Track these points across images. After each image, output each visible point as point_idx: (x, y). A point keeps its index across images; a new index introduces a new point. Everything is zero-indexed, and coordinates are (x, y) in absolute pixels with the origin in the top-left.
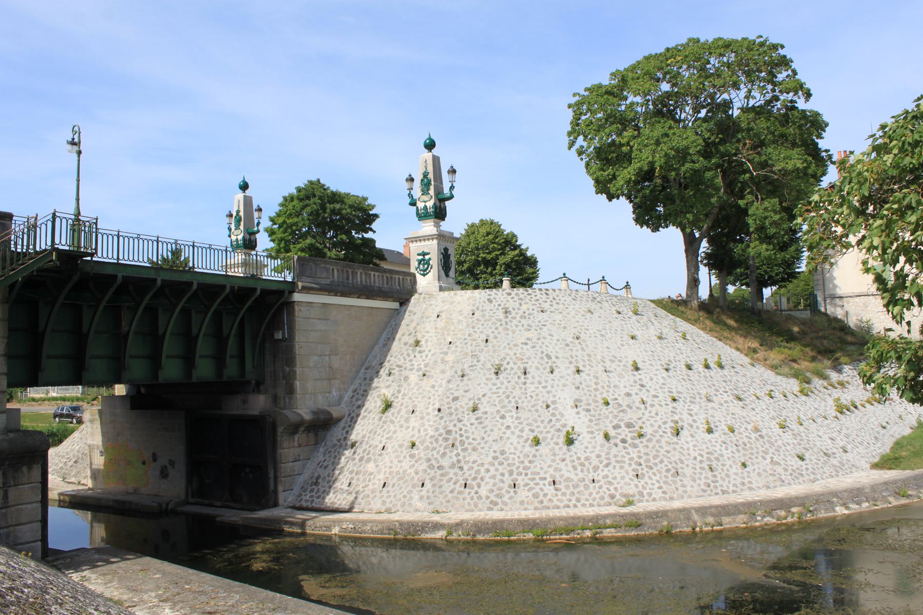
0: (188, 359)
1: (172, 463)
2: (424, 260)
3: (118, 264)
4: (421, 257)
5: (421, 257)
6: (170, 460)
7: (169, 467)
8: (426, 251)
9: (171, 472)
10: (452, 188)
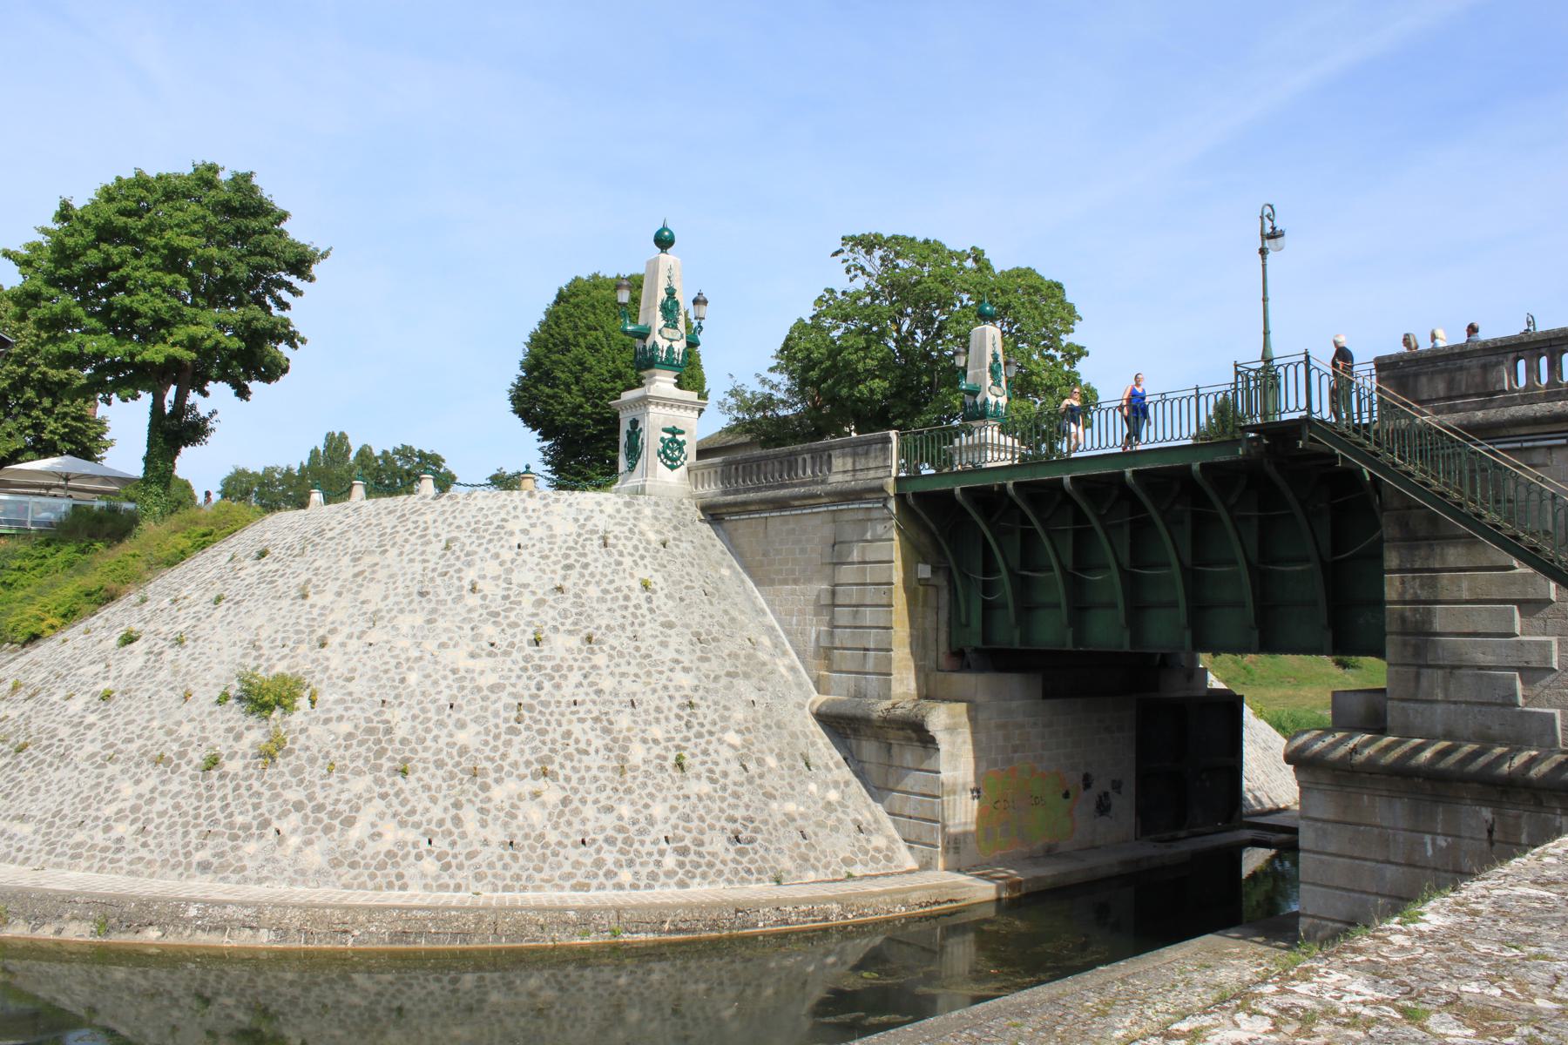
0: (1079, 609)
7: (1112, 793)
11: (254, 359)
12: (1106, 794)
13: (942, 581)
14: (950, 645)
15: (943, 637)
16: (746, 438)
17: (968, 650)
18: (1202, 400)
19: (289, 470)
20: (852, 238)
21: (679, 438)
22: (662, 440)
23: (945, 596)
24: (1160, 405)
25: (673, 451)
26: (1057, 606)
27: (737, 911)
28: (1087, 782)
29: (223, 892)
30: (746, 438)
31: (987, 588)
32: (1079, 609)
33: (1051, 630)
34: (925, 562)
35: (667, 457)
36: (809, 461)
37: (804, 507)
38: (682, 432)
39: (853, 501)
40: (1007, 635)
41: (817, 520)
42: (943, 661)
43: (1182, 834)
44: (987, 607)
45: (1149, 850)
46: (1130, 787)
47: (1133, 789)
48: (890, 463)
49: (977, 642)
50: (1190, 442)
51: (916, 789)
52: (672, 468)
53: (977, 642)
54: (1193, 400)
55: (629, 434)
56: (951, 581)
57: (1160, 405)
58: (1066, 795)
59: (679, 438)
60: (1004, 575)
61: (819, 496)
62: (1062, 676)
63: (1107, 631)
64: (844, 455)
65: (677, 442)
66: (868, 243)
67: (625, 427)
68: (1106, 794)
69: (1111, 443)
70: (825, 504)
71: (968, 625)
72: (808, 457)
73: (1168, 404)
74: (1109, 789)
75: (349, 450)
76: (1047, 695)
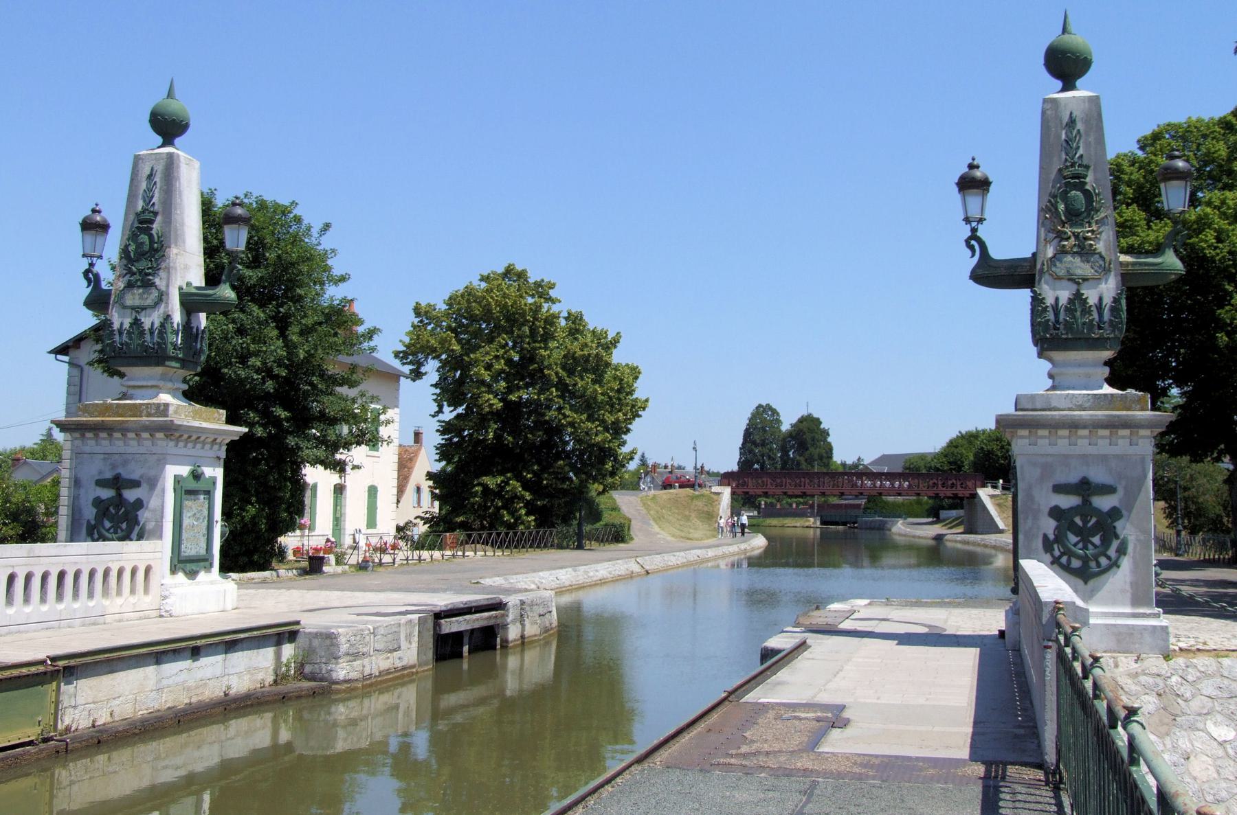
2: (1086, 509)
5: (1067, 502)
8: (1098, 475)
22: (1056, 512)
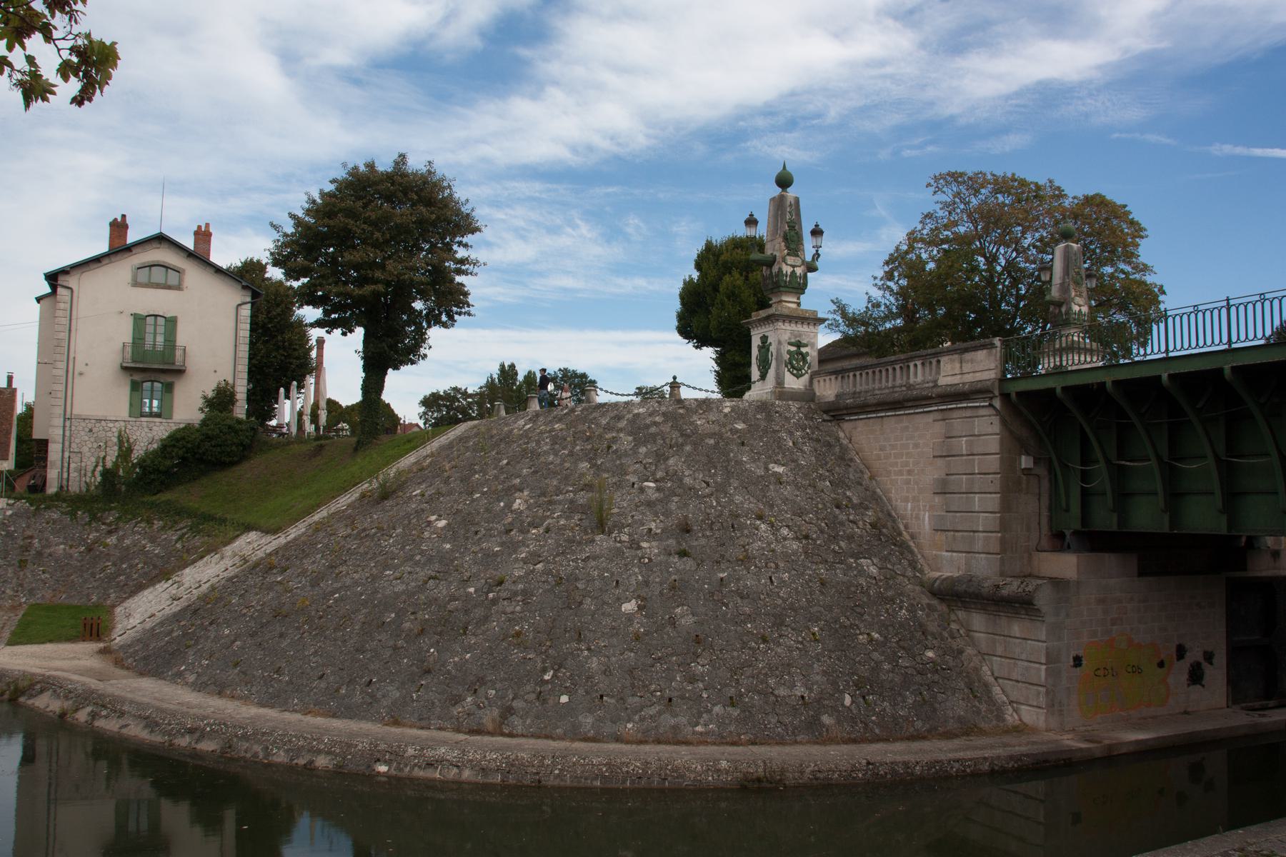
0: (1174, 497)
1: (1209, 657)
3: (1167, 359)
4: (793, 349)
6: (1205, 653)
7: (1205, 665)
9: (1208, 670)
10: (817, 256)
11: (449, 302)
12: (1199, 664)
13: (1042, 471)
14: (1051, 528)
15: (1044, 521)
16: (853, 350)
17: (1068, 533)
18: (1233, 310)
19: (1130, 213)
20: (942, 177)
21: (804, 350)
22: (789, 352)
23: (1045, 484)
24: (1259, 305)
25: (797, 360)
26: (1156, 494)
27: (869, 763)
28: (1181, 652)
29: (951, 751)
30: (853, 350)
31: (1085, 477)
32: (1174, 497)
33: (1147, 516)
34: (1028, 454)
35: (793, 367)
36: (919, 367)
37: (917, 407)
38: (806, 346)
39: (961, 401)
40: (1104, 519)
41: (930, 418)
42: (1045, 543)
43: (1272, 703)
44: (1085, 494)
45: (1239, 719)
46: (1221, 659)
47: (1224, 662)
48: (982, 366)
49: (1077, 525)
50: (1262, 342)
51: (1024, 657)
52: (798, 376)
53: (1077, 525)
54: (1224, 311)
55: (760, 348)
56: (1051, 470)
57: (1259, 305)
58: (1161, 665)
59: (804, 350)
60: (1102, 465)
61: (931, 398)
62: (1160, 557)
63: (1203, 516)
64: (952, 361)
65: (801, 354)
66: (955, 177)
67: (756, 342)
68: (1199, 664)
69: (1217, 341)
70: (936, 404)
71: (1067, 510)
72: (919, 363)
73: (1267, 304)
74: (1201, 659)
75: (516, 374)
76: (1142, 573)
